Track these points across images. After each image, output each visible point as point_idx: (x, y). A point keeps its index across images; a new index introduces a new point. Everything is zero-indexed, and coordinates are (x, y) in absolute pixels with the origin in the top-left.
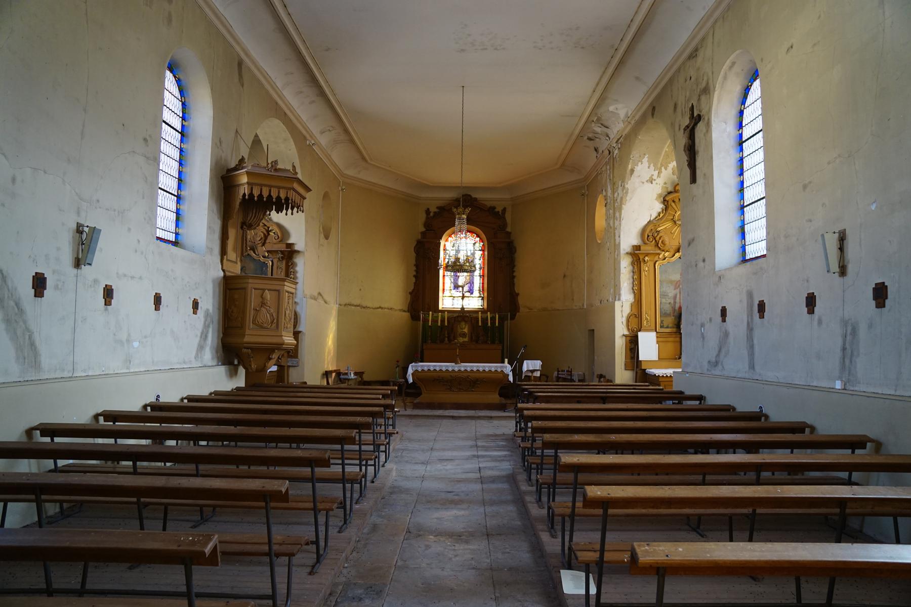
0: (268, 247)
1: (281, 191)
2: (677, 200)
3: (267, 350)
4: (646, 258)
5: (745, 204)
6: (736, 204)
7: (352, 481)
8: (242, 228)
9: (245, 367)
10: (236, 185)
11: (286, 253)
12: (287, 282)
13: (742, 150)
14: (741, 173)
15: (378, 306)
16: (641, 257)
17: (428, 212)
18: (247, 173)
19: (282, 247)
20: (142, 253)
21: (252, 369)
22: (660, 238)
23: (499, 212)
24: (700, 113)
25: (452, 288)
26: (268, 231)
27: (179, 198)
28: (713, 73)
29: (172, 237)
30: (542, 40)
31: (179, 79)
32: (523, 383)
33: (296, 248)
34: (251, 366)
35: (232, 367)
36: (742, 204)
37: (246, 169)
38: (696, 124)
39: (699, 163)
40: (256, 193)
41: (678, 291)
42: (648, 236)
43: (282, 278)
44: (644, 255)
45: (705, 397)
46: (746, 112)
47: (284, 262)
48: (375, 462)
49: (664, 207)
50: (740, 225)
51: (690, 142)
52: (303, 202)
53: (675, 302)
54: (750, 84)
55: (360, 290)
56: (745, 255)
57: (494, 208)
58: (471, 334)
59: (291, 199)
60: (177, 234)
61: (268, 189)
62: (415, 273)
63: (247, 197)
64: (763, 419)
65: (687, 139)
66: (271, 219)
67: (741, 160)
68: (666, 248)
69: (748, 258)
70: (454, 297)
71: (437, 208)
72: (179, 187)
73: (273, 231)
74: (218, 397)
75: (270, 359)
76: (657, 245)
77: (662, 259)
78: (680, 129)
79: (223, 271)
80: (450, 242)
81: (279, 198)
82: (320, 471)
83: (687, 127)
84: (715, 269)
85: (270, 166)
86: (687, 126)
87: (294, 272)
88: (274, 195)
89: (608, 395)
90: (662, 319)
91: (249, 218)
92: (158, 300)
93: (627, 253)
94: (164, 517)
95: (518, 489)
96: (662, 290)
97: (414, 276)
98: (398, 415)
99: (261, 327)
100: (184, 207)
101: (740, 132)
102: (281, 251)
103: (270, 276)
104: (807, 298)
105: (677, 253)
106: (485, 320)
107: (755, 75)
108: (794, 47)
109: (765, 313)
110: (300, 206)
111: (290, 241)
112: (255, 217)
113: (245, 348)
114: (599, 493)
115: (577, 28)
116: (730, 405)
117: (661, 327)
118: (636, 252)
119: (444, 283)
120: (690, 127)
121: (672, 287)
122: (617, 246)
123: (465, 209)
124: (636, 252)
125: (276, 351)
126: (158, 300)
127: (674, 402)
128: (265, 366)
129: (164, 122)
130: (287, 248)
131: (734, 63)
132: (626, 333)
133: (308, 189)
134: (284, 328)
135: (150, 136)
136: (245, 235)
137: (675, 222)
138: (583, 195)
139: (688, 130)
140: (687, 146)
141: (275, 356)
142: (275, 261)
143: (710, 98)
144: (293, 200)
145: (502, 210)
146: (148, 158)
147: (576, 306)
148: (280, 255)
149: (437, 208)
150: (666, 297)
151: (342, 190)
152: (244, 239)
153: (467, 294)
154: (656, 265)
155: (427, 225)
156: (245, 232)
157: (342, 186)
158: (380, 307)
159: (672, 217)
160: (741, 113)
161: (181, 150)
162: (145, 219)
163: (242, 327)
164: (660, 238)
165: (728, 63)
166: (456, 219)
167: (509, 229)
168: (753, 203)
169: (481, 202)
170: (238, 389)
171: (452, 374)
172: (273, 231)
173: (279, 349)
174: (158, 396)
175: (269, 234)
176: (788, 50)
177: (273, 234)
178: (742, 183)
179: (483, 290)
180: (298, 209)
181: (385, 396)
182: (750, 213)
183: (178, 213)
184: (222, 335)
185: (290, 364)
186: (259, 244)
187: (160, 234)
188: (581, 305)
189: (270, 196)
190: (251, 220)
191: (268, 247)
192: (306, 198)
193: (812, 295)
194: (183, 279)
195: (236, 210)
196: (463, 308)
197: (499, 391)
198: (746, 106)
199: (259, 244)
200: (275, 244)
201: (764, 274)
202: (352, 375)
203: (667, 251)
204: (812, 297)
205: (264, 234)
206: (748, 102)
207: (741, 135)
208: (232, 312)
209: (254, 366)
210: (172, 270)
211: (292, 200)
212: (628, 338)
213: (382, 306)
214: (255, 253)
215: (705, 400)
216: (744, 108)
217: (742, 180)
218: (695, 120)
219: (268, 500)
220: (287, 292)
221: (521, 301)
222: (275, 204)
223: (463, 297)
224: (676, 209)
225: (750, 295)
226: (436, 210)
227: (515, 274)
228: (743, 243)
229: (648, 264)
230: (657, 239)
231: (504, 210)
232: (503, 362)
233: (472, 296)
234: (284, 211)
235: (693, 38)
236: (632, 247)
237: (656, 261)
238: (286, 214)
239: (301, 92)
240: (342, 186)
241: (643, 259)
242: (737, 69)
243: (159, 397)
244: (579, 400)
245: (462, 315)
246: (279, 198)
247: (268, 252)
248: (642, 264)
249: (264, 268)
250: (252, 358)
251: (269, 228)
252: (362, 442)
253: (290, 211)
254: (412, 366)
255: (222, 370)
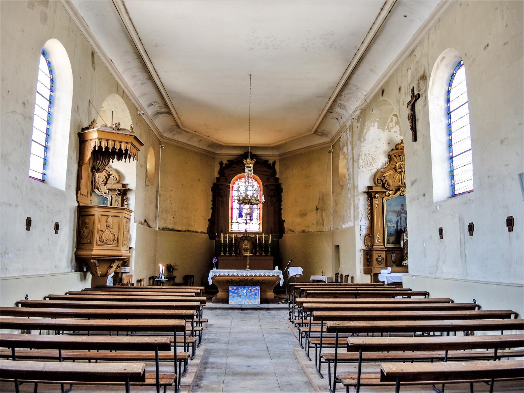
0: (109, 186)
1: (122, 144)
2: (397, 155)
3: (109, 261)
4: (377, 195)
5: (453, 156)
6: (446, 155)
7: (180, 360)
8: (92, 171)
9: (92, 273)
10: (87, 140)
11: (122, 191)
12: (126, 210)
13: (450, 118)
14: (450, 134)
15: (186, 230)
16: (373, 194)
17: (221, 163)
18: (98, 131)
19: (119, 186)
20: (18, 187)
21: (97, 274)
22: (386, 181)
23: (270, 164)
24: (419, 93)
25: (238, 217)
26: (109, 175)
27: (46, 148)
28: (428, 65)
29: (40, 177)
30: (308, 42)
31: (49, 62)
32: (294, 284)
33: (129, 187)
34: (96, 272)
35: (82, 273)
36: (451, 155)
37: (97, 128)
38: (416, 100)
39: (419, 126)
40: (104, 145)
41: (399, 218)
42: (378, 180)
43: (119, 207)
44: (375, 193)
45: (429, 293)
46: (452, 92)
47: (120, 197)
48: (193, 345)
49: (389, 160)
50: (450, 170)
51: (412, 113)
52: (138, 153)
53: (397, 226)
54: (455, 72)
55: (174, 218)
56: (455, 191)
57: (267, 161)
58: (252, 249)
59: (129, 150)
60: (44, 174)
61: (113, 143)
62: (212, 206)
63: (97, 148)
64: (477, 308)
65: (410, 110)
66: (111, 167)
67: (450, 125)
68: (390, 188)
69: (457, 193)
70: (239, 223)
71: (228, 161)
72: (47, 141)
73: (113, 175)
74: (71, 296)
75: (111, 267)
76: (383, 186)
77: (387, 195)
78: (403, 104)
79: (78, 202)
80: (236, 184)
81: (120, 149)
82: (161, 354)
83: (410, 102)
84: (433, 201)
85: (114, 126)
86: (410, 102)
87: (127, 205)
88: (117, 147)
89: (359, 292)
90: (388, 238)
91: (97, 164)
92: (29, 223)
93: (364, 192)
94: (35, 390)
95: (299, 363)
96: (388, 218)
97: (212, 208)
98: (204, 308)
99: (105, 243)
100: (50, 155)
101: (448, 105)
102: (119, 189)
103: (110, 206)
104: (507, 220)
105: (398, 192)
106: (260, 239)
107: (459, 65)
108: (489, 46)
109: (514, 227)
110: (135, 156)
111: (125, 183)
112: (101, 165)
113: (93, 259)
114: (394, 369)
115: (333, 34)
116: (449, 299)
117: (388, 243)
118: (369, 191)
119: (232, 213)
120: (412, 102)
121: (395, 215)
122: (355, 187)
123: (252, 160)
124: (369, 191)
125: (116, 261)
126: (29, 223)
127: (404, 296)
128: (107, 272)
129: (38, 92)
130: (122, 187)
131: (444, 58)
132: (364, 248)
133: (142, 144)
134: (123, 244)
135: (27, 101)
136: (94, 176)
137: (396, 170)
138: (329, 152)
139: (411, 104)
140: (410, 116)
141: (115, 265)
142: (114, 196)
143: (426, 82)
144: (131, 152)
145: (273, 163)
146: (25, 117)
147: (325, 229)
148: (118, 192)
149: (228, 161)
150: (391, 222)
151: (162, 147)
152: (93, 178)
153: (248, 221)
154: (384, 200)
155: (221, 172)
156: (94, 174)
157: (162, 145)
158: (188, 231)
159: (394, 167)
160: (449, 92)
161: (49, 113)
162: (21, 162)
163: (91, 243)
164: (386, 181)
165: (440, 57)
166: (246, 168)
167: (277, 176)
168: (460, 154)
169: (259, 157)
170: (86, 290)
171: (241, 278)
172: (113, 175)
173: (119, 260)
174: (27, 296)
175: (109, 177)
176: (485, 48)
177: (113, 177)
178: (451, 140)
179: (259, 218)
180: (134, 158)
181: (197, 294)
182: (457, 162)
183: (45, 160)
184: (75, 250)
185: (123, 271)
186: (102, 184)
187: (31, 174)
188: (329, 228)
189: (114, 148)
190: (99, 165)
191: (109, 186)
192: (139, 151)
193: (511, 218)
194: (48, 207)
195: (88, 158)
196: (246, 231)
197: (274, 289)
198: (452, 87)
199: (102, 184)
200: (114, 184)
201: (472, 204)
202: (163, 278)
203: (391, 190)
204: (511, 219)
205: (106, 177)
206: (454, 85)
207: (449, 108)
208: (84, 232)
209: (99, 272)
210: (40, 201)
211: (130, 151)
212: (366, 252)
213: (189, 230)
214: (99, 191)
215: (429, 295)
216: (451, 89)
217: (450, 139)
218: (416, 97)
219: (128, 380)
220: (125, 218)
221: (286, 225)
222: (117, 154)
223: (246, 223)
224: (397, 161)
225: (461, 219)
226: (228, 163)
227: (282, 207)
228: (453, 183)
229: (378, 199)
230: (384, 181)
231: (274, 163)
232: (274, 269)
233: (252, 222)
234: (124, 160)
235: (413, 41)
236: (367, 188)
237: (384, 197)
238: (125, 162)
239: (136, 76)
240: (162, 145)
241: (374, 196)
242: (445, 62)
243: (28, 296)
244: (335, 295)
245: (246, 236)
246: (120, 149)
247: (109, 190)
248: (374, 199)
249: (106, 202)
250: (98, 266)
251: (109, 172)
252: (335, 346)
253: (128, 159)
254: (212, 272)
255: (77, 275)
